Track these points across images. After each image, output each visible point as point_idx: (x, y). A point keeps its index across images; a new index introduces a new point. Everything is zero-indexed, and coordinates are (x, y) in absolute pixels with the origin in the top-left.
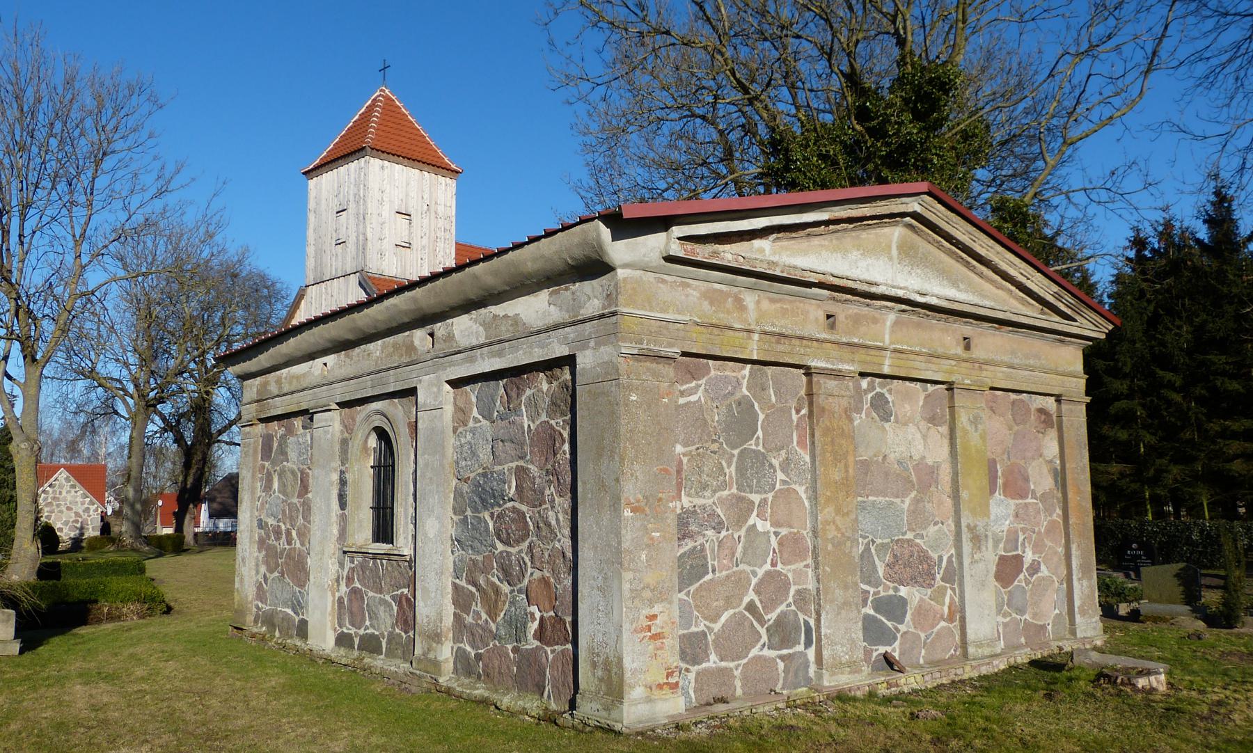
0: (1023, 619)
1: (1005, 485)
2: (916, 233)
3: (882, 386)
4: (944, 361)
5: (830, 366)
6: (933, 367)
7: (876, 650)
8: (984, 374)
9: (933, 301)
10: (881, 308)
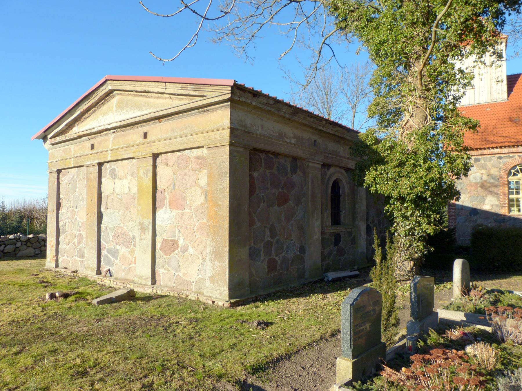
0: (176, 274)
1: (171, 203)
2: (121, 95)
3: (114, 165)
4: (132, 148)
5: (91, 163)
6: (127, 152)
7: (107, 267)
8: (153, 147)
9: (114, 125)
10: (106, 134)
